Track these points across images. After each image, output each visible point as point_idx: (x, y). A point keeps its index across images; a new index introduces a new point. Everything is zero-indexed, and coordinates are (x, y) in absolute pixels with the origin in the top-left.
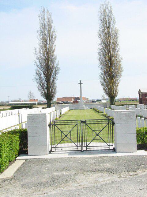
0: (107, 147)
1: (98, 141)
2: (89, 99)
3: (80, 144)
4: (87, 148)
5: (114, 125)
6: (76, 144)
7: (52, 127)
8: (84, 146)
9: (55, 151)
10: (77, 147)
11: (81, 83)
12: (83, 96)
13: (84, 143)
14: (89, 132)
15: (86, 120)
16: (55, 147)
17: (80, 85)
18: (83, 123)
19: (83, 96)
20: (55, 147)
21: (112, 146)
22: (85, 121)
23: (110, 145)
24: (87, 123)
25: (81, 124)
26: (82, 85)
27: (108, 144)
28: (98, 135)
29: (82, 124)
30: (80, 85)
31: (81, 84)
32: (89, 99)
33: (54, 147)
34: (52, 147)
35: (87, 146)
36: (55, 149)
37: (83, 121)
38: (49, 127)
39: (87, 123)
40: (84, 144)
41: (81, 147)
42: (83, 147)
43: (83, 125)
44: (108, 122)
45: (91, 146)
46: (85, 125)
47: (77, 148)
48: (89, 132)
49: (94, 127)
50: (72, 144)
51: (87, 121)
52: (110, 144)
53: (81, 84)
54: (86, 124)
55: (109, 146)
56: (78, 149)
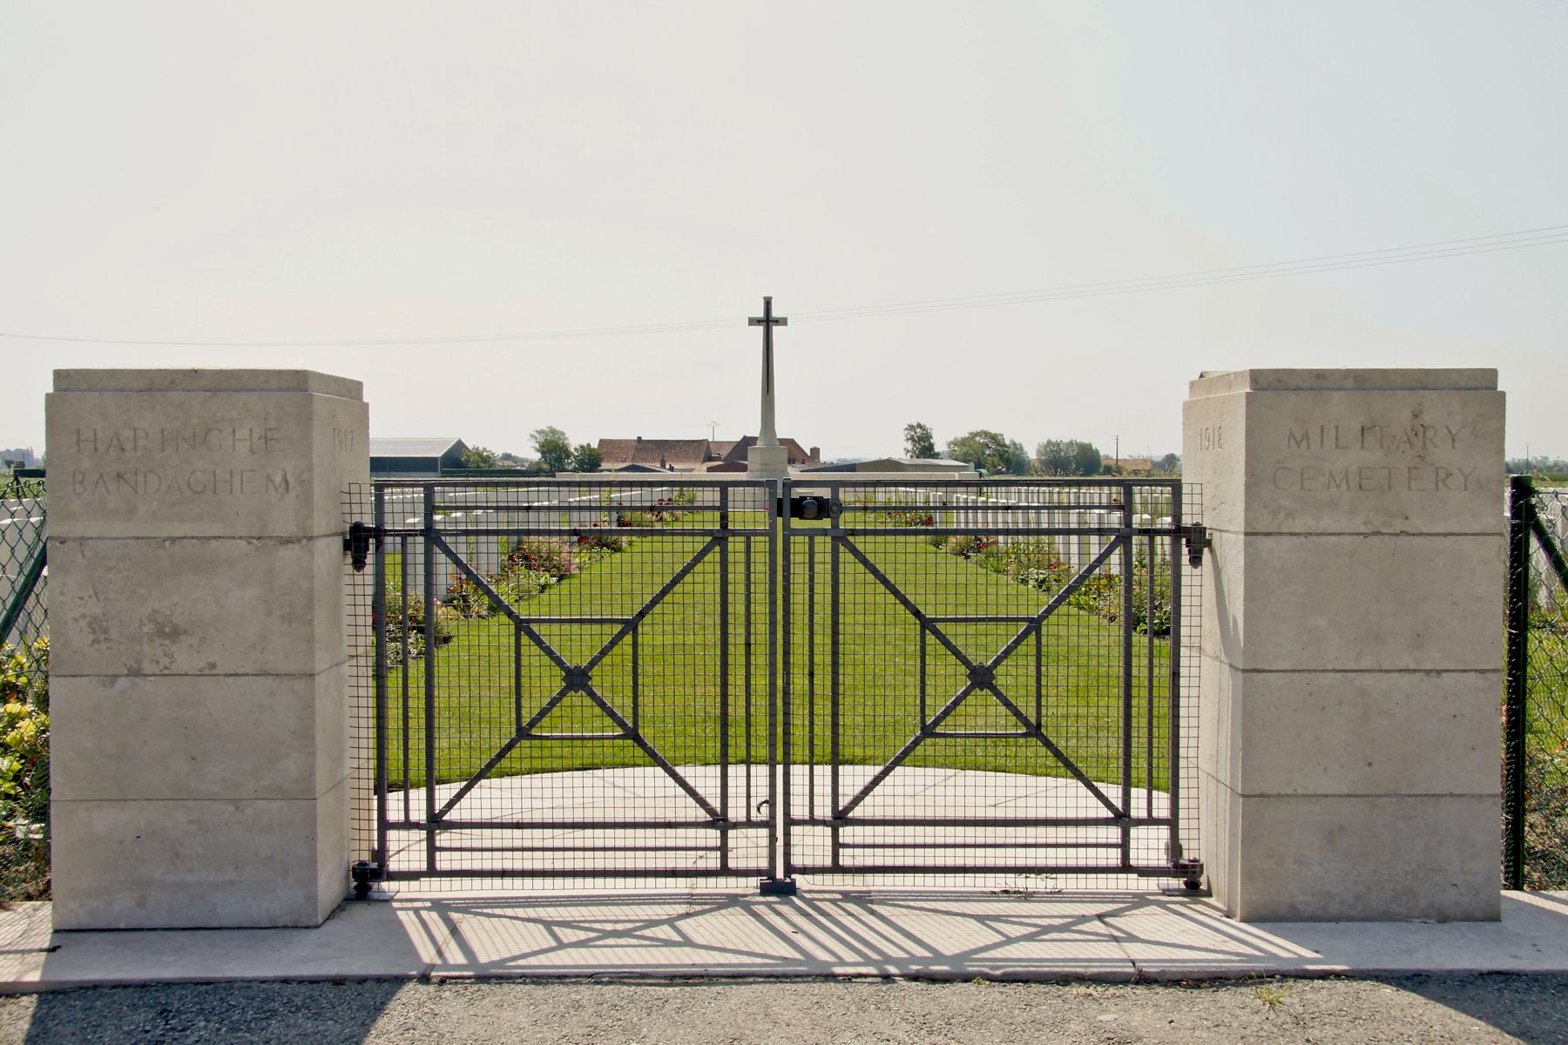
0: (1091, 834)
1: (983, 754)
2: (826, 457)
3: (748, 786)
4: (837, 846)
5: (1196, 560)
6: (705, 779)
7: (392, 560)
8: (799, 811)
9: (432, 872)
10: (720, 821)
11: (775, 314)
12: (782, 432)
13: (799, 772)
14: (874, 625)
15: (835, 486)
16: (435, 822)
17: (760, 329)
18: (796, 523)
19: (782, 432)
20: (435, 822)
21: (1164, 832)
22: (825, 493)
23: (1138, 810)
24: (847, 521)
25: (771, 534)
26: (776, 329)
27: (1114, 793)
28: (981, 678)
29: (789, 533)
30: (760, 329)
31: (768, 322)
32: (826, 457)
33: (419, 814)
34: (385, 825)
35: (840, 818)
36: (432, 849)
37: (798, 492)
38: (359, 564)
39: (847, 521)
40: (810, 787)
41: (770, 824)
42: (790, 822)
43: (799, 544)
44: (1115, 519)
45: (879, 814)
46: (823, 544)
47: (736, 545)
48: (874, 625)
49: (938, 579)
50: (642, 789)
51: (846, 496)
52: (1138, 795)
53: (768, 322)
54: (841, 538)
55: (1122, 818)
56: (812, 821)
